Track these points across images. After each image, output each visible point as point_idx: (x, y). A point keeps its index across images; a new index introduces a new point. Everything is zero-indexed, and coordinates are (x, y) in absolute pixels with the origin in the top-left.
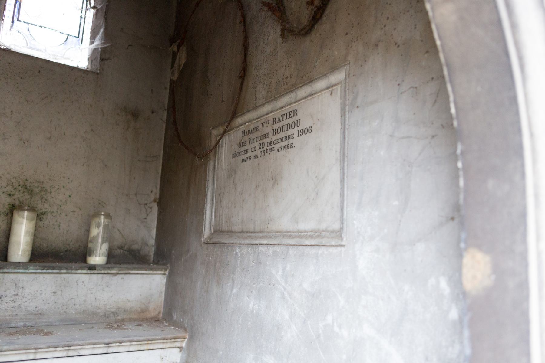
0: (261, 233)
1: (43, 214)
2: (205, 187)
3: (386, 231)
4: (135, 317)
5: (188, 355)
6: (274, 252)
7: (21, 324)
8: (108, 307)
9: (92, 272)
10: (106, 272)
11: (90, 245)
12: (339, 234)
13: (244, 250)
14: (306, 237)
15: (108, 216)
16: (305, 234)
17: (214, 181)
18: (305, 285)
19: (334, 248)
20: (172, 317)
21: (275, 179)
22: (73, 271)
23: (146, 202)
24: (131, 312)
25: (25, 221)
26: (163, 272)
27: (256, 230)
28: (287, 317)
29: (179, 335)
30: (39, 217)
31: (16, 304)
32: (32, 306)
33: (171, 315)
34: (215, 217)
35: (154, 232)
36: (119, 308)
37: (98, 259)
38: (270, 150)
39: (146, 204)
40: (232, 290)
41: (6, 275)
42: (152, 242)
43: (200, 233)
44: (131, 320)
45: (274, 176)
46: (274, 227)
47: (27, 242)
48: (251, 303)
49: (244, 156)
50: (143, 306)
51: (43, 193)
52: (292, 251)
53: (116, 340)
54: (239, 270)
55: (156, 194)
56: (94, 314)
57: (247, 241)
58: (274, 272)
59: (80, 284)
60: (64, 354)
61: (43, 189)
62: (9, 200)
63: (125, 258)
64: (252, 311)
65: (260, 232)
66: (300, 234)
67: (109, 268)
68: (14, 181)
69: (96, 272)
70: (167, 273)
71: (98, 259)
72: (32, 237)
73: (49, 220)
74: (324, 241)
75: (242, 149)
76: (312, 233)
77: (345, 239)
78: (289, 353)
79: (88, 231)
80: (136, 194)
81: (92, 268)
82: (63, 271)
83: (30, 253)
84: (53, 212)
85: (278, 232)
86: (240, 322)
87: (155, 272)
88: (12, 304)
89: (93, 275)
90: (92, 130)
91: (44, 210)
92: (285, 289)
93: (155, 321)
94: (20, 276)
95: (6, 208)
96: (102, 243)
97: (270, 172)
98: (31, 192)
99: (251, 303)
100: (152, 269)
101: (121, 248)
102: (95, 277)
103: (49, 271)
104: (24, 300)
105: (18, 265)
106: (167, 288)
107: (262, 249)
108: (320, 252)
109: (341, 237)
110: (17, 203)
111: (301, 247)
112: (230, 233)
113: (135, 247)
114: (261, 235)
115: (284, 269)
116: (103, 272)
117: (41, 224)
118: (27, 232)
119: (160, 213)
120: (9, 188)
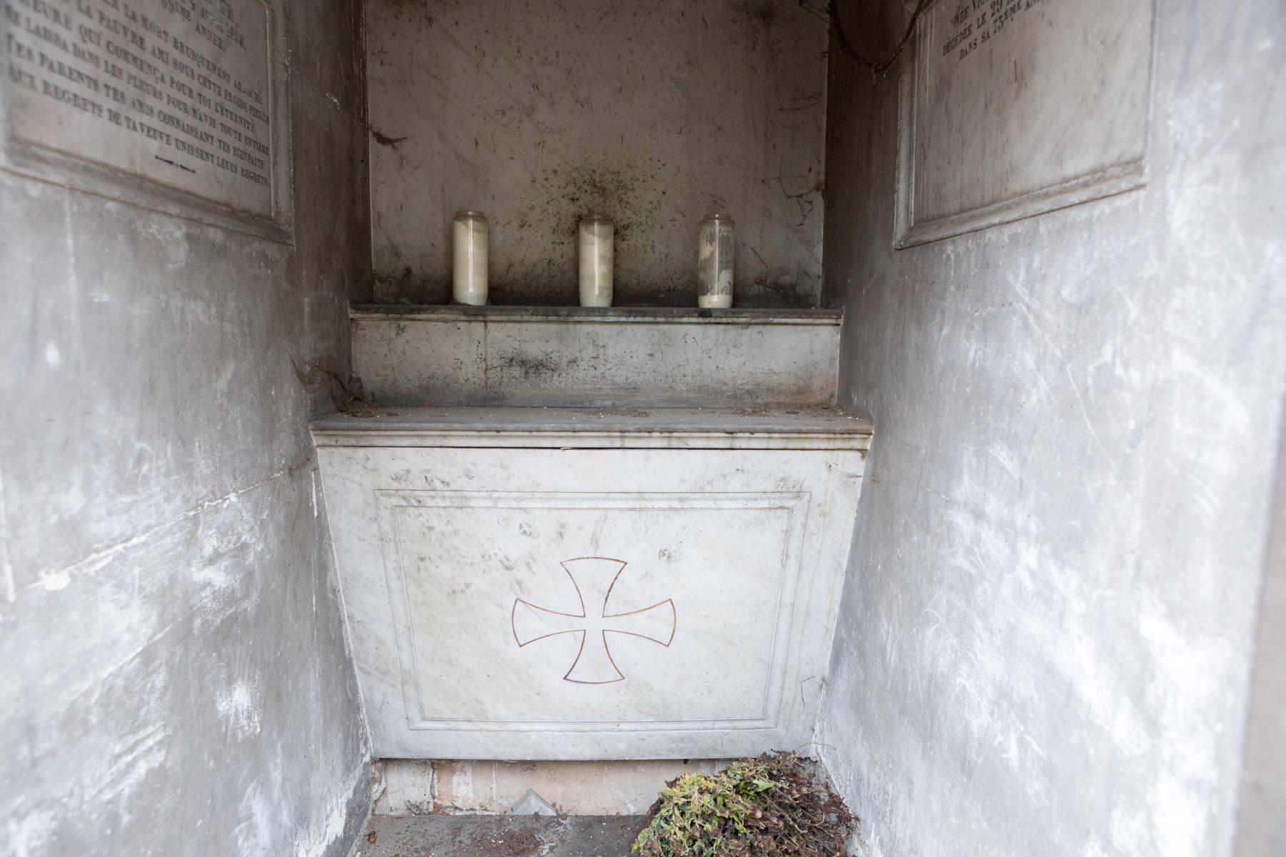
0: (995, 203)
1: (626, 227)
2: (896, 132)
3: (1236, 123)
4: (787, 400)
5: (875, 464)
6: (1012, 237)
7: (610, 403)
8: (739, 382)
9: (707, 320)
10: (730, 320)
11: (702, 276)
12: (1134, 165)
13: (962, 245)
14: (1073, 189)
15: (727, 221)
16: (1075, 182)
17: (911, 117)
18: (1066, 293)
19: (1124, 196)
20: (849, 403)
21: (1020, 77)
22: (676, 320)
23: (801, 191)
24: (780, 392)
25: (596, 240)
26: (833, 321)
27: (986, 201)
28: (1031, 364)
29: (858, 427)
30: (618, 234)
31: (598, 372)
32: (621, 376)
33: (850, 396)
34: (916, 192)
35: (819, 250)
36: (758, 384)
37: (716, 299)
38: (1013, 10)
39: (801, 196)
40: (941, 331)
41: (578, 326)
42: (817, 269)
43: (889, 232)
44: (779, 406)
45: (1019, 67)
46: (1017, 185)
47: (603, 274)
48: (971, 350)
49: (964, 45)
50: (801, 383)
51: (621, 191)
52: (1044, 225)
53: (743, 427)
54: (952, 288)
55: (818, 173)
56: (718, 393)
57: (967, 228)
58: (1010, 278)
59: (690, 341)
60: (665, 444)
61: (621, 185)
62: (573, 209)
63: (765, 297)
64: (973, 365)
65: (993, 202)
66: (1066, 185)
67: (734, 315)
68: (574, 175)
69: (712, 320)
70: (841, 322)
71: (716, 299)
72: (611, 267)
73: (635, 239)
74: (1105, 188)
75: (961, 28)
76: (1088, 178)
77: (1147, 170)
78: (1033, 433)
79: (697, 252)
80: (779, 177)
81: (706, 313)
82: (659, 319)
83: (611, 292)
84: (640, 224)
85: (1021, 195)
86: (954, 389)
87: (818, 321)
88: (592, 372)
89: (709, 327)
90: (689, 62)
91: (626, 222)
92: (1029, 308)
93: (825, 407)
94: (598, 328)
95: (568, 224)
96: (720, 272)
97: (1012, 64)
98: (603, 191)
99: (971, 350)
100: (811, 316)
101: (760, 282)
102: (712, 329)
103: (639, 319)
104: (609, 366)
105: (592, 311)
106: (844, 349)
107: (991, 235)
108: (1096, 213)
109: (1139, 171)
110: (585, 212)
111: (1059, 214)
112: (941, 217)
113: (786, 280)
114: (992, 207)
115: (1029, 267)
116: (724, 320)
117: (623, 245)
118: (602, 257)
119: (828, 209)
120: (571, 188)
